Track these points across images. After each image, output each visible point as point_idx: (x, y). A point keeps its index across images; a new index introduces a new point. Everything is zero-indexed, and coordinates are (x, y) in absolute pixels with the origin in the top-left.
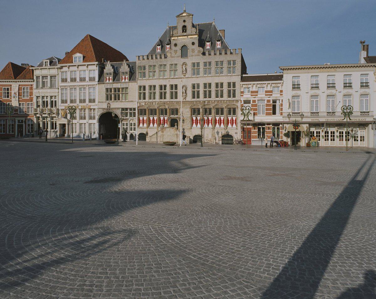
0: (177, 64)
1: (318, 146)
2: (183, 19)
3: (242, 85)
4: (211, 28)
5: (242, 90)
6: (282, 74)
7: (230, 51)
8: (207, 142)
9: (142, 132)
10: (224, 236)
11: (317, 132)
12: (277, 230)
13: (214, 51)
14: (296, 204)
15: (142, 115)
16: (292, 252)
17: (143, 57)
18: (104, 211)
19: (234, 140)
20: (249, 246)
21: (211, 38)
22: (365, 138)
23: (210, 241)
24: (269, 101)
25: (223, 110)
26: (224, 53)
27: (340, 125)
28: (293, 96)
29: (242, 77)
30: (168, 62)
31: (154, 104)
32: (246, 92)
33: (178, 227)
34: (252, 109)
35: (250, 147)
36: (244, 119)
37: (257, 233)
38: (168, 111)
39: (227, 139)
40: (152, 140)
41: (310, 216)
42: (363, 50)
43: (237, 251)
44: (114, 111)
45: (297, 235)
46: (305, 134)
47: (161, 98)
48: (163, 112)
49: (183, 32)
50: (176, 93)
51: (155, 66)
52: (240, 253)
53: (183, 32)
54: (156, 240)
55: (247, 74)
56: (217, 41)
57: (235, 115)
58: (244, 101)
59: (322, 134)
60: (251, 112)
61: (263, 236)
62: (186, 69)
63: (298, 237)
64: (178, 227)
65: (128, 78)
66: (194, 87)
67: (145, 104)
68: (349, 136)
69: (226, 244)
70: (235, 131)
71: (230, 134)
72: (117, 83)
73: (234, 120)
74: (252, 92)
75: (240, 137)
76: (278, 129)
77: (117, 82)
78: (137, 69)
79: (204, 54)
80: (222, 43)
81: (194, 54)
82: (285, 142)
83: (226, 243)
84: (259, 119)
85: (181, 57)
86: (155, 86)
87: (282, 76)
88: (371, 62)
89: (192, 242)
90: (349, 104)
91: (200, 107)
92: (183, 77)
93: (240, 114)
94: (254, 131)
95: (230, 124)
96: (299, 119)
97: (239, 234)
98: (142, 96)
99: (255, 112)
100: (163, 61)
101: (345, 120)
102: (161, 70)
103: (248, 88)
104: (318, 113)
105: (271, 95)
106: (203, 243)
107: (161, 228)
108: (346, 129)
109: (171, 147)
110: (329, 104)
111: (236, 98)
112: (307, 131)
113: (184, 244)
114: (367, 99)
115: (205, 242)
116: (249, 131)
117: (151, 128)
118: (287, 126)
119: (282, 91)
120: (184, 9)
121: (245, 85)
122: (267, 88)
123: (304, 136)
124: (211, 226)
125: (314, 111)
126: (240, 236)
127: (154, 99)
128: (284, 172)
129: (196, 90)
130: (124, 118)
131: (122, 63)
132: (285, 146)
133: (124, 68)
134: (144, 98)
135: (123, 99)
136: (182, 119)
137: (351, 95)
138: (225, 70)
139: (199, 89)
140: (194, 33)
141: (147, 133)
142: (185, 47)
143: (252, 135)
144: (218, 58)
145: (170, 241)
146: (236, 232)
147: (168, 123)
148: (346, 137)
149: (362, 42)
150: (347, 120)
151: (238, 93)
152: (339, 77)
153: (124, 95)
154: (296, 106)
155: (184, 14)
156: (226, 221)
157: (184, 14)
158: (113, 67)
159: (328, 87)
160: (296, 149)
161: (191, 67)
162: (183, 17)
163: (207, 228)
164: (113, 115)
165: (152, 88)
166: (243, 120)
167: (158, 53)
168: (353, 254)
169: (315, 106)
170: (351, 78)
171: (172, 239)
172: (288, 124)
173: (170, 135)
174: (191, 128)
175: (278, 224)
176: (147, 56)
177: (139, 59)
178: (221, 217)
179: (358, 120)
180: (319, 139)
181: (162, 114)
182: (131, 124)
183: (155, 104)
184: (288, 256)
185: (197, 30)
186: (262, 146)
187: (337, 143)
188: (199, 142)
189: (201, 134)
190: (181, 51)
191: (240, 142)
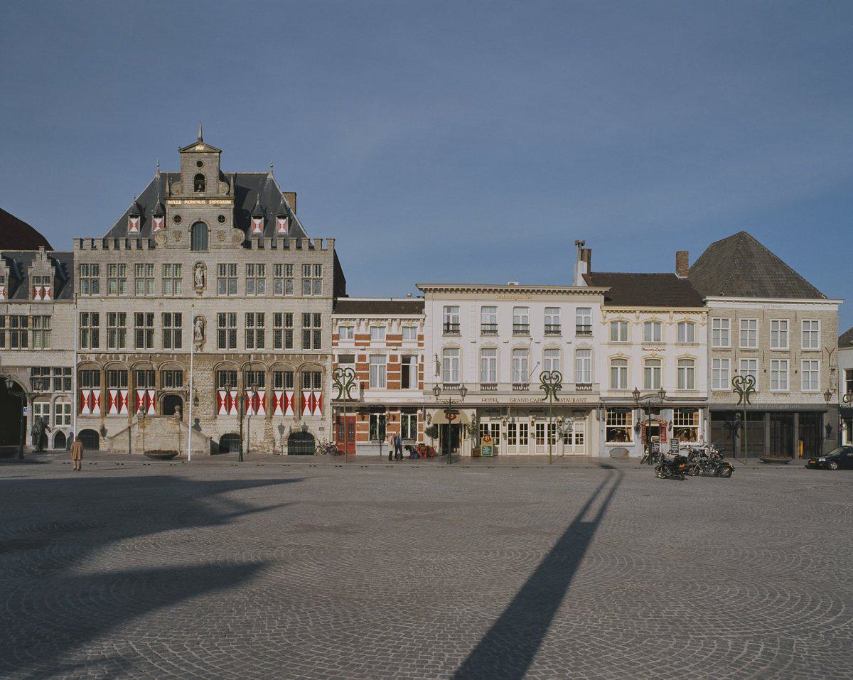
0: (180, 265)
1: (496, 455)
2: (197, 158)
3: (334, 321)
4: (264, 183)
5: (335, 332)
6: (423, 300)
7: (309, 243)
8: (254, 450)
9: (83, 429)
10: (302, 647)
11: (493, 425)
12: (411, 625)
13: (272, 240)
14: (448, 574)
15: (88, 386)
16: (439, 663)
17: (93, 243)
18: (9, 619)
19: (317, 444)
20: (356, 661)
21: (263, 208)
22: (584, 441)
23: (271, 660)
24: (393, 358)
25: (292, 376)
26: (295, 246)
27: (538, 411)
28: (444, 349)
29: (335, 303)
30: (159, 258)
31: (121, 360)
32: (343, 336)
33: (199, 638)
34: (359, 374)
35: (353, 459)
36: (339, 396)
37: (371, 636)
38: (158, 376)
39: (301, 442)
40: (115, 447)
41: (476, 595)
42: (582, 260)
43: (330, 672)
44: (12, 374)
45: (449, 632)
46: (469, 430)
47: (139, 344)
48: (145, 378)
49: (195, 191)
50: (179, 333)
51: (125, 267)
52: (338, 675)
53: (195, 191)
54: (149, 669)
55: (347, 296)
56: (279, 217)
57: (319, 387)
58: (339, 356)
59: (504, 430)
60: (355, 381)
61: (383, 641)
62: (203, 277)
63: (452, 636)
64: (199, 638)
65: (52, 292)
66: (222, 320)
67: (97, 359)
68: (554, 433)
69: (308, 663)
70: (319, 424)
71: (308, 431)
72: (20, 303)
73: (317, 399)
74: (358, 337)
75: (331, 439)
76: (414, 418)
77: (19, 300)
78: (76, 272)
79: (247, 245)
80: (290, 222)
81: (222, 243)
82: (428, 447)
83: (306, 660)
84: (371, 397)
85: (192, 250)
86: (123, 316)
87: (422, 305)
88: (596, 285)
89: (232, 666)
90: (554, 367)
91: (237, 367)
92: (195, 295)
93: (331, 386)
94: (363, 425)
95: (307, 408)
96: (456, 398)
97: (335, 640)
98: (89, 336)
99: (365, 381)
100: (146, 255)
101: (548, 401)
102: (168, 276)
103: (349, 328)
104: (496, 385)
105: (400, 345)
106: (258, 666)
107: (157, 644)
108: (548, 419)
109: (164, 462)
110: (518, 367)
111: (323, 350)
112: (473, 423)
113: (216, 671)
114: (587, 358)
115: (261, 664)
116: (351, 425)
117: (113, 418)
118: (432, 412)
119: (423, 336)
120: (200, 136)
121: (343, 322)
122: (390, 330)
123: (467, 434)
124: (273, 630)
125: (488, 382)
126: (336, 645)
127: (122, 345)
128: (427, 512)
129: (227, 327)
130: (40, 392)
131: (35, 254)
132: (428, 456)
133: (41, 266)
134: (96, 344)
135: (37, 343)
136: (193, 396)
137: (558, 349)
138: (297, 284)
139: (235, 325)
140: (225, 194)
141: (104, 431)
142: (201, 225)
143: (360, 434)
144: (281, 256)
145: (183, 669)
146: (328, 637)
147: (158, 405)
148: (549, 436)
149: (579, 244)
150: (550, 400)
151: (325, 338)
152: (536, 311)
153: (39, 335)
154: (451, 370)
155: (199, 148)
156: (305, 618)
157: (199, 148)
158: (9, 262)
159: (515, 332)
160: (451, 463)
161: (215, 273)
162: (196, 154)
163: (264, 635)
164: (7, 384)
165: (117, 320)
166: (338, 400)
167: (131, 236)
168: (550, 657)
169: (489, 370)
170: (590, 315)
171: (186, 665)
172: (434, 408)
173: (160, 433)
174: (216, 418)
175: (413, 615)
176: (104, 240)
177: (81, 247)
178: (294, 611)
179: (571, 401)
180: (498, 440)
181: (141, 384)
182: (59, 407)
183: (124, 359)
184: (431, 672)
185: (232, 187)
186: (380, 458)
187: (533, 449)
188: (235, 451)
189: (239, 430)
190: (192, 235)
191: (329, 449)
